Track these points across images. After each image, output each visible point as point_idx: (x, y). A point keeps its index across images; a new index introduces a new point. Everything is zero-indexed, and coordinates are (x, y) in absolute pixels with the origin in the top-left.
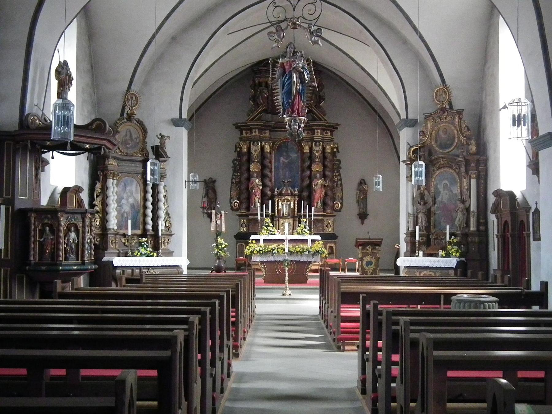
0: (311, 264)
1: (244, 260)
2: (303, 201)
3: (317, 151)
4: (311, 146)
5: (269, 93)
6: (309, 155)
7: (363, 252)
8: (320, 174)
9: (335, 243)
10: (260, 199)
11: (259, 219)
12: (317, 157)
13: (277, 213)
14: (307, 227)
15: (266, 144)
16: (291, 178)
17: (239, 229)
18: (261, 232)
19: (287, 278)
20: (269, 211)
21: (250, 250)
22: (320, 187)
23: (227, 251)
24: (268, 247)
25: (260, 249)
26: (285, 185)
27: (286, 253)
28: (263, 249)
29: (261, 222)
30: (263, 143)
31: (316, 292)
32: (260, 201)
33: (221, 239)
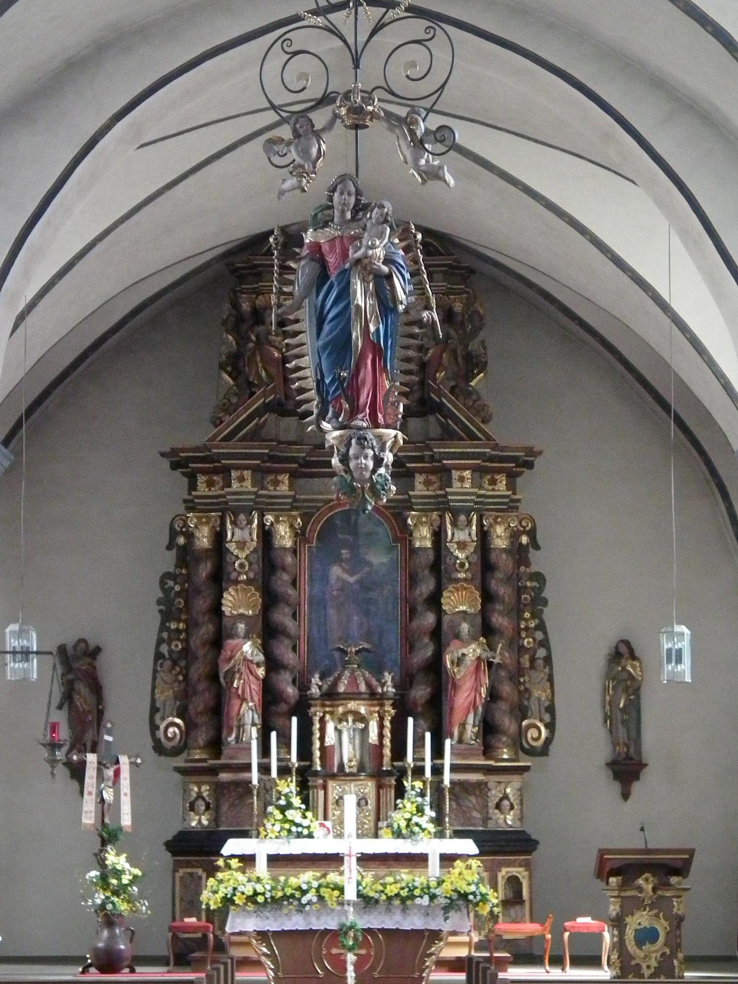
0: (440, 940)
2: (410, 720)
3: (462, 545)
4: (440, 527)
6: (431, 556)
8: (472, 625)
9: (527, 865)
10: (260, 712)
11: (255, 781)
12: (462, 565)
14: (427, 809)
16: (367, 637)
18: (261, 829)
21: (221, 895)
22: (472, 668)
24: (286, 880)
25: (255, 891)
26: (349, 663)
28: (268, 887)
29: (262, 794)
30: (269, 518)
32: (257, 721)
33: (118, 854)
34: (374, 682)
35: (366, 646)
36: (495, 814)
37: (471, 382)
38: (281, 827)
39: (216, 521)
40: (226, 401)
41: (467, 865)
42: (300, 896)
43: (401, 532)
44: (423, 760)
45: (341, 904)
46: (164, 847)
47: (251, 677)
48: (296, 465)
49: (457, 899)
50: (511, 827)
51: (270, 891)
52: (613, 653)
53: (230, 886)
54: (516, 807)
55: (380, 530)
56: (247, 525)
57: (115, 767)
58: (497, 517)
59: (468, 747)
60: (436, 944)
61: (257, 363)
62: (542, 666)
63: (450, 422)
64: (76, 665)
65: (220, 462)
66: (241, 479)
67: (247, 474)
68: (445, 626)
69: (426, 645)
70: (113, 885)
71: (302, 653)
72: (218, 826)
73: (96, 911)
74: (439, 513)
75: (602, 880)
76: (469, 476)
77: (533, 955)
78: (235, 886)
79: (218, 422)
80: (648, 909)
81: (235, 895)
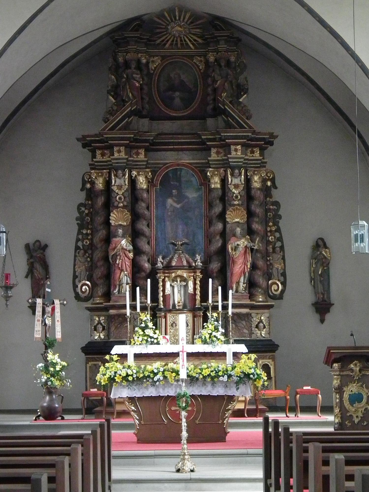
0: (234, 401)
1: (100, 394)
2: (210, 280)
3: (236, 186)
4: (225, 177)
5: (143, 80)
6: (220, 193)
7: (342, 376)
8: (242, 229)
9: (273, 359)
10: (131, 277)
11: (128, 314)
12: (237, 197)
13: (161, 303)
14: (220, 328)
15: (139, 175)
16: (187, 237)
17: (91, 336)
18: (132, 340)
19: (184, 434)
20: (146, 299)
21: (107, 376)
22: (243, 252)
23: (67, 377)
24: (145, 367)
25: (127, 373)
26: (176, 250)
27: (182, 380)
28: (135, 371)
29: (132, 321)
30: (134, 173)
31: (246, 463)
32: (129, 282)
33: (54, 354)
34: (191, 260)
35: (186, 241)
36: (256, 331)
37: (240, 99)
38: (143, 339)
39: (106, 174)
40: (110, 109)
41: (249, 357)
42: (153, 377)
43: (204, 180)
44: (218, 302)
45: (178, 381)
46: (81, 351)
47: (126, 258)
48: (148, 144)
49: (244, 377)
50: (264, 338)
51: (136, 374)
52: (315, 244)
53: (113, 371)
54: (266, 327)
55: (193, 179)
56: (123, 176)
57: (52, 306)
58: (255, 171)
59: (240, 294)
60: (231, 403)
61: (127, 90)
62: (279, 251)
63: (229, 119)
64: (34, 254)
65: (108, 142)
66: (119, 151)
67: (122, 149)
68: (228, 230)
69: (218, 240)
70: (51, 371)
71: (153, 246)
72: (109, 339)
73: (42, 386)
74: (225, 169)
75: (328, 365)
76: (240, 149)
77: (277, 406)
78: (116, 371)
79: (107, 120)
80: (356, 383)
81: (116, 376)
